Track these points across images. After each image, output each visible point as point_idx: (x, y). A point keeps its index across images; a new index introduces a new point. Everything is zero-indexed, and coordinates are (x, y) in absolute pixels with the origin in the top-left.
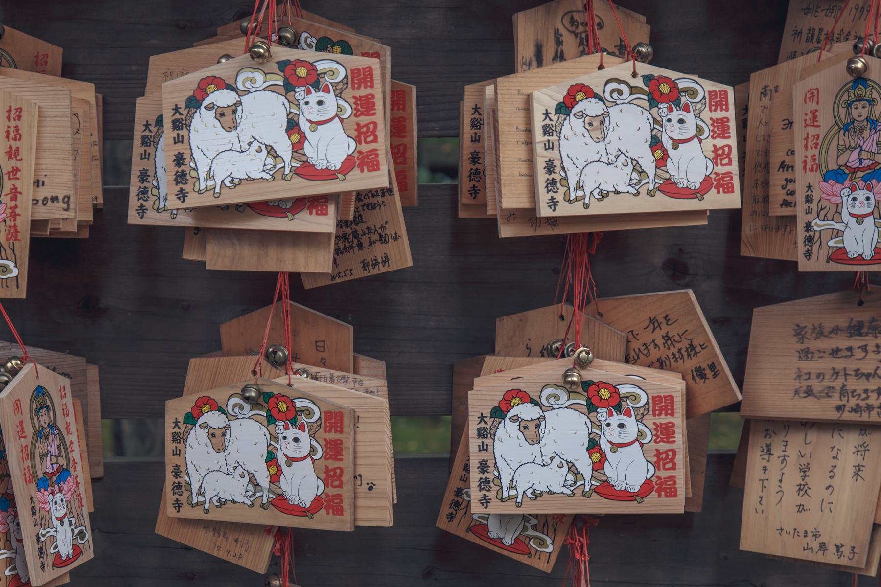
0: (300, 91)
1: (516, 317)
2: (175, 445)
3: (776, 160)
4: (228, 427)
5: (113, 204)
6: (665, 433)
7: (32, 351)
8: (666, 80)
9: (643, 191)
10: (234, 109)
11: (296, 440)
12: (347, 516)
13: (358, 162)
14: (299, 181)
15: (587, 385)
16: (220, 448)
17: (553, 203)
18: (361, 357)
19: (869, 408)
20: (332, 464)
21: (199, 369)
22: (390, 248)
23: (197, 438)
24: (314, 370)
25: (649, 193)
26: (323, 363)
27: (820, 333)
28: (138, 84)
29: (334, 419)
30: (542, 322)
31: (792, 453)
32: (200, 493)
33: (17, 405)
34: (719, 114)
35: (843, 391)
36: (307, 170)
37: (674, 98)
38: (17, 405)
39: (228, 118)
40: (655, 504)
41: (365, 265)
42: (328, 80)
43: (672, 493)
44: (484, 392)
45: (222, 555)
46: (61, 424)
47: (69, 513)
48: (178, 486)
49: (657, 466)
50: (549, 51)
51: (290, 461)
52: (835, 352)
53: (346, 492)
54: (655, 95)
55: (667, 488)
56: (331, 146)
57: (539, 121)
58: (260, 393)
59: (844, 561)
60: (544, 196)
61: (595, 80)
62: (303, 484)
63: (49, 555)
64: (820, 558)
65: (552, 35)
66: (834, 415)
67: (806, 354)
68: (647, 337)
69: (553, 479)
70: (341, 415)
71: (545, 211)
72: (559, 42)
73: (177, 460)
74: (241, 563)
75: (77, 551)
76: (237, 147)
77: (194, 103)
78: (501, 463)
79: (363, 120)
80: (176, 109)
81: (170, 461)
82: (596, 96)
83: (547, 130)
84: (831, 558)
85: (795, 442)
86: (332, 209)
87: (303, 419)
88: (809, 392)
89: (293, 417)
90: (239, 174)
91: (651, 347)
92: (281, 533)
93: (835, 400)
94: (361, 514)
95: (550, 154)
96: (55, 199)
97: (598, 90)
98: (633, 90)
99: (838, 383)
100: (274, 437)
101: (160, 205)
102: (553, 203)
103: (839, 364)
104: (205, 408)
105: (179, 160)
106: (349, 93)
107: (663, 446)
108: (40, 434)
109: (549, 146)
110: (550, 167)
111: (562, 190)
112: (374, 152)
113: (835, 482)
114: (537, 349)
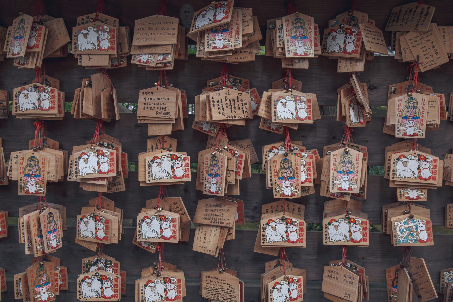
1: (150, 200)
3: (201, 171)
5: (65, 176)
6: (175, 226)
7: (49, 204)
8: (175, 155)
9: (169, 178)
10: (87, 159)
12: (109, 241)
14: (99, 174)
15: (160, 216)
16: (87, 226)
17: (149, 180)
18: (116, 208)
19: (217, 222)
20: (107, 230)
21: (84, 209)
22: (121, 187)
24: (106, 210)
25: (171, 178)
26: (108, 209)
27: (210, 206)
28: (70, 153)
29: (107, 221)
30: (154, 202)
31: (203, 231)
33: (44, 217)
34: (187, 162)
35: (212, 219)
36: (100, 172)
37: (177, 158)
38: (44, 217)
39: (86, 161)
40: (172, 241)
41: (117, 190)
42: (106, 154)
43: (176, 238)
44: (140, 217)
45: (87, 247)
46: (55, 220)
47: (56, 238)
48: (79, 233)
49: (173, 233)
50: (154, 147)
52: (212, 210)
53: (109, 236)
54: (173, 158)
55: (175, 238)
56: (105, 168)
57: (147, 164)
58: (94, 215)
59: (210, 254)
60: (147, 179)
61: (159, 155)
62: (101, 234)
64: (206, 253)
65: (155, 144)
66: (210, 224)
67: (207, 210)
68: (173, 206)
69: (153, 235)
70: (108, 221)
71: (148, 182)
72: (157, 145)
73: (78, 228)
74: (91, 249)
75: (58, 246)
77: (80, 158)
78: (143, 231)
80: (76, 159)
81: (77, 228)
82: (159, 158)
83: (148, 165)
84: (208, 253)
85: (204, 228)
86: (106, 180)
87: (102, 221)
88: (206, 219)
89: (100, 220)
90: (88, 173)
92: (98, 244)
93: (211, 221)
94: (112, 241)
95: (149, 170)
96: (51, 176)
97: (160, 157)
98: (168, 157)
99: (212, 217)
100: (96, 224)
101: (73, 178)
102: (149, 180)
103: (213, 213)
105: (76, 169)
106: (109, 157)
107: (174, 229)
108: (49, 222)
109: (149, 169)
110: (149, 173)
111: (151, 177)
112: (113, 169)
113: (210, 237)
114: (153, 207)
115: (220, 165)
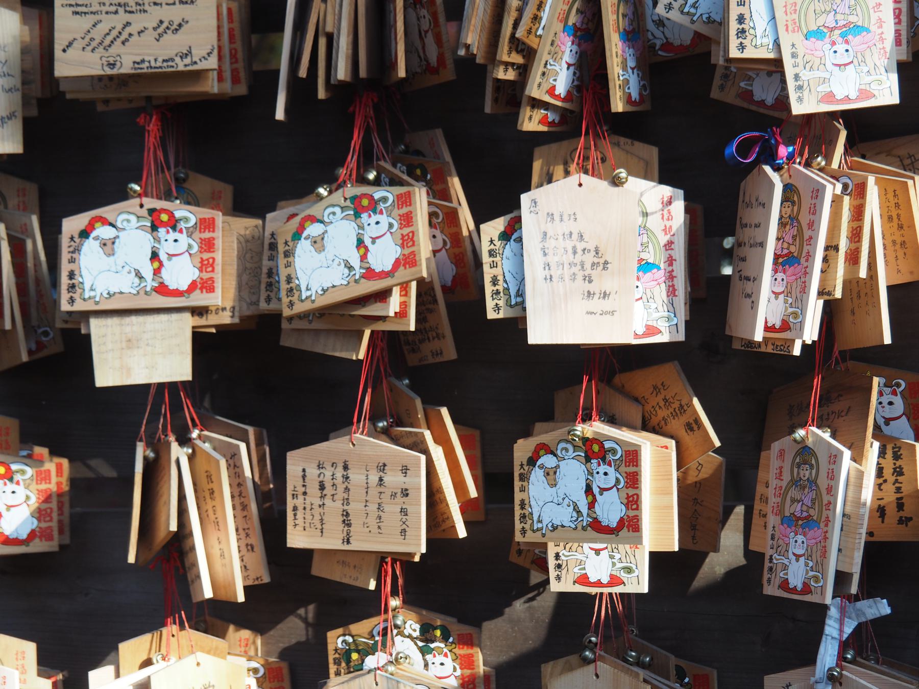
0: (162, 231)
2: (521, 483)
4: (558, 467)
11: (606, 474)
13: (199, 286)
23: (537, 475)
32: (540, 521)
36: (162, 289)
51: (603, 490)
63: (778, 577)
76: (114, 269)
79: (206, 256)
91: (657, 408)
104: (542, 452)
106: (197, 235)
115: (823, 482)
